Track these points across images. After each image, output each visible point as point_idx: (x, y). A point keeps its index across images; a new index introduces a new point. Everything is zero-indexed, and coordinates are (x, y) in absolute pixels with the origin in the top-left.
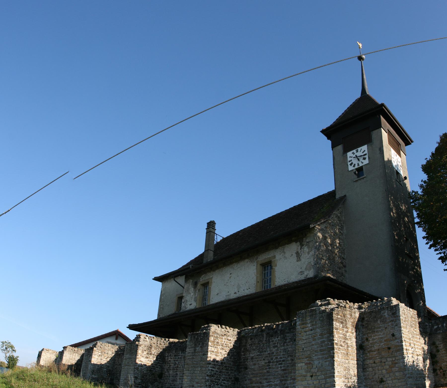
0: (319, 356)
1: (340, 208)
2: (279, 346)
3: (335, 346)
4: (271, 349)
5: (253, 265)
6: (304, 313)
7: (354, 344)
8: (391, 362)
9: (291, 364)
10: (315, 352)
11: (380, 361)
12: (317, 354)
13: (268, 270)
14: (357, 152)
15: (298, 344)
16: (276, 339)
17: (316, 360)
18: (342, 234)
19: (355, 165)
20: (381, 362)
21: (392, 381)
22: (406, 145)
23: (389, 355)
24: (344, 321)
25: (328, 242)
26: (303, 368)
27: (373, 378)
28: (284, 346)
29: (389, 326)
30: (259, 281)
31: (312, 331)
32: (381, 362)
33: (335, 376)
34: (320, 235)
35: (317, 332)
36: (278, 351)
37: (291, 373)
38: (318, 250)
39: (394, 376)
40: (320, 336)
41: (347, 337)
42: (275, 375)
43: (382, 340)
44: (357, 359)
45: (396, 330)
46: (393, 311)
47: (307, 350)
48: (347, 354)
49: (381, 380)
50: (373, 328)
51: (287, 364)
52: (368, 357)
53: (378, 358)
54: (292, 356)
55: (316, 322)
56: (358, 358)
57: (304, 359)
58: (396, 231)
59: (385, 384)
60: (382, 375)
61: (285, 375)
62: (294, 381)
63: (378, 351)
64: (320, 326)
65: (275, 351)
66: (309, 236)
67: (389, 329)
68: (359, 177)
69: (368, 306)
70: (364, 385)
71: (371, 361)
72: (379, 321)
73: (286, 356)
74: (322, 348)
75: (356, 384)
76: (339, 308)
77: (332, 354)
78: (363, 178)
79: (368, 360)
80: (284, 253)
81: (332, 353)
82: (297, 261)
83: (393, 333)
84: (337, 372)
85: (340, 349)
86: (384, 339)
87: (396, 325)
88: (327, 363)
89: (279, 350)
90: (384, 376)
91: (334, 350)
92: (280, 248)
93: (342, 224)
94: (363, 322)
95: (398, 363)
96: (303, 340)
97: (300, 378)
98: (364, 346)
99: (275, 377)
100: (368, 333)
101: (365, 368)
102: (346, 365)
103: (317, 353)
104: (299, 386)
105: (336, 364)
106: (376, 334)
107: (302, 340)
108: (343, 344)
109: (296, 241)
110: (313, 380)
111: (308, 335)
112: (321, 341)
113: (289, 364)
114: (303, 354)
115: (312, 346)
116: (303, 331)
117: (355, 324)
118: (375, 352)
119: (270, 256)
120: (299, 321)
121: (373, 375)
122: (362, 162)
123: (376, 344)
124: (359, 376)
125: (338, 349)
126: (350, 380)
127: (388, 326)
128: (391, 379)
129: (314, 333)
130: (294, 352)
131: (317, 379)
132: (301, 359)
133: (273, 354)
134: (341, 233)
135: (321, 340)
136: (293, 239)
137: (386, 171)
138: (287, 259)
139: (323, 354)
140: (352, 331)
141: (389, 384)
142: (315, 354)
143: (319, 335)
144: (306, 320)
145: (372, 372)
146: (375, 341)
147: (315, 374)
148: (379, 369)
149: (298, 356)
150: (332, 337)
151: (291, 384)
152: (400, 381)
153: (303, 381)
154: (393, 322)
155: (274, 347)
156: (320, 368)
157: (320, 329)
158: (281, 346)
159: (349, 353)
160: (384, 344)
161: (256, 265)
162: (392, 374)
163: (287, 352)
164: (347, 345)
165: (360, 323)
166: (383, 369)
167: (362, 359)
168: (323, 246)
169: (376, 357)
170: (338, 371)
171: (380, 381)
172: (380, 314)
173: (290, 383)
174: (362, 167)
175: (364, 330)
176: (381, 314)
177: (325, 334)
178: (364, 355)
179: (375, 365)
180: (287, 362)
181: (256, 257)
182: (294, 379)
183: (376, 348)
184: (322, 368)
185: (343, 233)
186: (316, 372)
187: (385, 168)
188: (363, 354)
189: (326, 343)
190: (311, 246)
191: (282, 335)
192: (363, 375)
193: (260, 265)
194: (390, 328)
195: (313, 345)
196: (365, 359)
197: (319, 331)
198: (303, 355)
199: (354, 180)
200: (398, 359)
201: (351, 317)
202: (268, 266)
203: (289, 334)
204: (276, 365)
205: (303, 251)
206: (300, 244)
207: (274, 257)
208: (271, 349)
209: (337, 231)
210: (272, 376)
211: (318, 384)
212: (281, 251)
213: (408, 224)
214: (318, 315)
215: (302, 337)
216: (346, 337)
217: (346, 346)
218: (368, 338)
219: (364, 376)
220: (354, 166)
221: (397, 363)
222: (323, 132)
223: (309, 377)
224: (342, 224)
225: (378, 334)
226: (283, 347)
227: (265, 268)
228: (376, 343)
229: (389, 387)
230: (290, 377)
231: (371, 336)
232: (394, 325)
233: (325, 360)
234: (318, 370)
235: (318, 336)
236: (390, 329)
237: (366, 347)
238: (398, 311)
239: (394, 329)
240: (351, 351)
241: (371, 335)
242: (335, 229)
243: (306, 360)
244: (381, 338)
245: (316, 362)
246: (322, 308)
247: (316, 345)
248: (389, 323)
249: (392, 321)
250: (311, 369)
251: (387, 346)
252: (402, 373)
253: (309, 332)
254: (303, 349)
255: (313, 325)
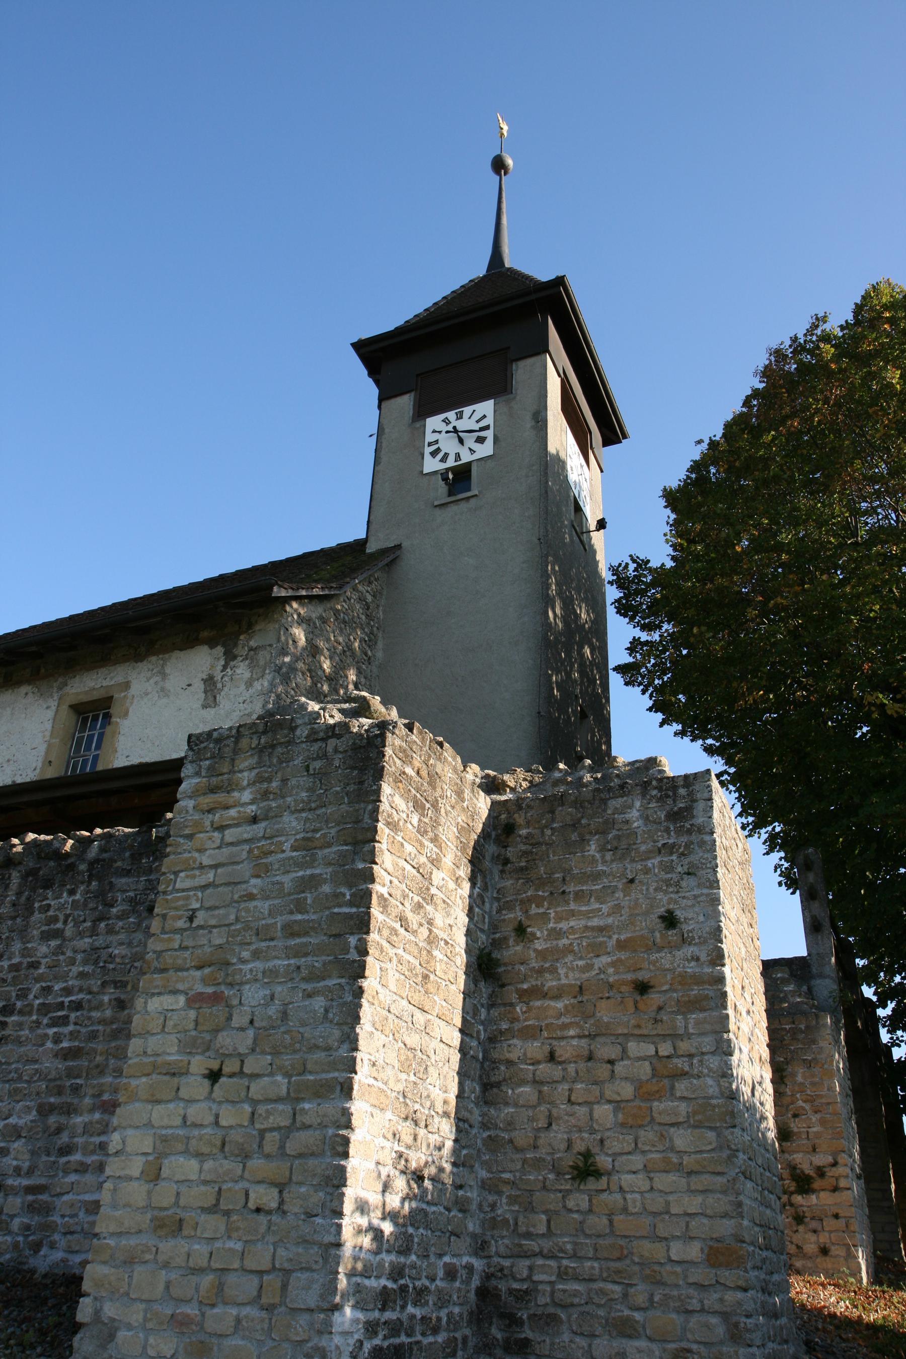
0: (278, 958)
1: (376, 580)
2: (68, 933)
3: (375, 911)
4: (29, 945)
5: (45, 706)
6: (228, 737)
7: (461, 940)
8: (647, 1063)
9: (112, 1023)
10: (258, 934)
11: (586, 1053)
12: (268, 947)
13: (93, 728)
14: (458, 419)
15: (170, 888)
16: (62, 901)
17: (256, 980)
18: (369, 658)
19: (446, 455)
20: (590, 1058)
21: (651, 1179)
22: (607, 442)
23: (638, 1026)
24: (428, 805)
25: (321, 667)
26: (170, 1023)
27: (535, 1147)
28: (94, 932)
29: (647, 871)
30: (52, 760)
31: (255, 827)
32: (590, 1058)
33: (356, 1087)
34: (299, 634)
35: (280, 833)
36: (61, 957)
37: (101, 1070)
38: (286, 680)
39: (661, 1148)
40: (294, 854)
41: (433, 891)
42: (20, 1079)
43: (601, 939)
44: (464, 1020)
45: (687, 894)
46: (674, 801)
47: (213, 922)
48: (426, 977)
49: (581, 1164)
50: (557, 875)
51: (92, 1025)
52: (517, 1026)
53: (572, 1033)
54: (124, 984)
55: (284, 781)
56: (468, 1018)
57: (185, 974)
58: (558, 672)
59: (604, 1191)
60: (593, 1131)
61: (68, 1084)
62: (106, 1117)
63: (575, 997)
64: (303, 802)
65: (46, 957)
66: (260, 630)
67: (647, 889)
68: (455, 495)
69: (531, 782)
70: (483, 1181)
71: (535, 1048)
72: (593, 847)
73: (93, 982)
74: (299, 917)
75: (448, 1167)
76: (415, 731)
77: (353, 955)
78: (468, 498)
79: (515, 1041)
80: (164, 676)
81: (356, 948)
82: (205, 707)
83: (670, 912)
84: (366, 1062)
85: (395, 938)
86: (615, 937)
87: (689, 874)
88: (319, 1003)
89: (63, 953)
90: (602, 1141)
91: (368, 932)
92: (153, 659)
93: (375, 629)
94: (505, 847)
95: (693, 1076)
96: (201, 867)
97: (144, 1079)
98: (497, 963)
99: (17, 1091)
100: (530, 900)
101: (493, 1079)
102: (413, 1040)
103: (263, 944)
104: (130, 1132)
105: (369, 1017)
106: (573, 906)
107: (193, 869)
108: (413, 919)
109: (212, 643)
110: (220, 1103)
111: (232, 844)
112: (303, 877)
113: (99, 1023)
114: (189, 943)
115: (243, 905)
116: (208, 823)
117: (472, 843)
118: (557, 997)
119: (112, 683)
120: (198, 774)
121: (539, 1130)
122: (470, 449)
123: (570, 958)
124: (464, 1121)
125: (386, 932)
126: (422, 1132)
127: (646, 873)
128: (641, 1167)
129: (264, 837)
130: (136, 964)
131: (243, 1094)
132: (171, 972)
133: (32, 970)
134: (366, 654)
135: (301, 873)
136: (205, 634)
137: (547, 482)
138: (168, 696)
139: (299, 952)
140: (456, 870)
141: (628, 1196)
142: (253, 947)
143: (294, 849)
144: (232, 772)
145: (534, 1107)
146: (565, 941)
147: (239, 1063)
148: (573, 1098)
149: (159, 954)
150: (365, 861)
151: (91, 1135)
152: (698, 1182)
153: (158, 1102)
154: (674, 857)
155: (46, 936)
156: (274, 1028)
157: (304, 815)
158: (81, 935)
159: (432, 977)
160: (613, 964)
161: (54, 708)
162: (651, 1135)
163: (105, 962)
164: (430, 931)
165: (492, 849)
166: (602, 1099)
167: (485, 1030)
168: (303, 674)
169: (565, 1027)
170: (373, 1059)
171: (575, 1167)
172: (605, 810)
173: (87, 1130)
174: (468, 465)
175: (509, 883)
176: (609, 812)
177: (329, 845)
178: (495, 1012)
179: (556, 1072)
180: (94, 1014)
181: (60, 680)
182: (110, 1107)
183: (564, 981)
184: (282, 1029)
185: (372, 659)
186: (243, 1050)
187: (546, 473)
188: (491, 1006)
189: (326, 889)
190: (262, 663)
191: (94, 883)
192: (480, 1119)
193: (71, 706)
194: (655, 885)
195: (251, 897)
196: (501, 1033)
197: (294, 824)
198: (186, 948)
199: (436, 503)
200: (693, 1051)
201: (457, 803)
202: (95, 719)
203: (131, 880)
204: (38, 1027)
205: (232, 675)
206: (225, 654)
207: (127, 685)
208: (29, 945)
209: (357, 644)
210: (8, 1081)
211: (241, 1126)
212: (152, 670)
213: (592, 671)
214: (304, 745)
215: (196, 855)
216: (428, 889)
217: (424, 932)
218: (526, 922)
219: (485, 1126)
220: (444, 459)
221: (684, 1074)
222: (360, 347)
223: (199, 1078)
224: (375, 629)
225: (584, 908)
226: (91, 936)
227: (85, 720)
228: (572, 951)
229: (625, 1210)
230: (94, 1096)
231: (544, 913)
232: (680, 869)
233: (309, 987)
234: (255, 1040)
235: (283, 851)
236: (651, 890)
237: (510, 968)
238: (701, 805)
239: (678, 892)
240: (443, 966)
241: (541, 910)
242: (350, 635)
243: (195, 981)
244: (601, 929)
245: (253, 995)
246: (327, 715)
247: (267, 898)
248: (649, 858)
249: (670, 849)
250: (217, 1031)
251: (629, 977)
252: (711, 1135)
253: (239, 829)
254: (191, 919)
255: (265, 795)
